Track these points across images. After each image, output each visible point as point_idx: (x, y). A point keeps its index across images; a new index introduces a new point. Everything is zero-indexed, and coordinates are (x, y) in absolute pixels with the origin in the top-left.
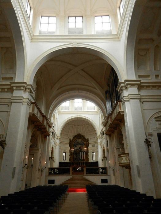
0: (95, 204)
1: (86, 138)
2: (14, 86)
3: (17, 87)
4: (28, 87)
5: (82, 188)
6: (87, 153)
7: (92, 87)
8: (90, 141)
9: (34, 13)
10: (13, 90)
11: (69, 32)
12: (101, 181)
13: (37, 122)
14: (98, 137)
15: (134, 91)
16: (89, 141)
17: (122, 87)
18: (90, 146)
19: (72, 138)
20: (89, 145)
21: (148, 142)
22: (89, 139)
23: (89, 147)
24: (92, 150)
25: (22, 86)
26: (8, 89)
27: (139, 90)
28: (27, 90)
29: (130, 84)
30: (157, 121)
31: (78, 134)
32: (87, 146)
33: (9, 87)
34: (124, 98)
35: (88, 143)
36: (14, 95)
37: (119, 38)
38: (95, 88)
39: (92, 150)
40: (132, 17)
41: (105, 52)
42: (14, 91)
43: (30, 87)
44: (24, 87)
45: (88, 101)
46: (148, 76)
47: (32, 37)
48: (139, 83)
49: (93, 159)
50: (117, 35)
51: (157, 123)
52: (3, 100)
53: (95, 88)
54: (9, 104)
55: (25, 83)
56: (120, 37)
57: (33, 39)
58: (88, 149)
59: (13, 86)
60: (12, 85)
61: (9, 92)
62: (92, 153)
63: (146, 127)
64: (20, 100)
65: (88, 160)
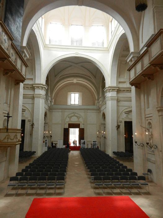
0: (88, 168)
2: (35, 87)
3: (37, 87)
4: (44, 87)
5: (141, 17)
7: (89, 76)
9: (45, 22)
10: (34, 98)
11: (72, 42)
12: (21, 121)
13: (12, 72)
15: (114, 94)
21: (118, 127)
25: (40, 87)
26: (31, 87)
27: (117, 93)
28: (43, 89)
29: (112, 89)
30: (125, 114)
33: (31, 86)
36: (35, 93)
37: (108, 50)
38: (90, 77)
40: (117, 43)
41: (98, 62)
42: (35, 90)
44: (41, 87)
46: (124, 82)
48: (118, 88)
50: (107, 48)
51: (125, 115)
52: (27, 95)
53: (90, 77)
54: (33, 98)
55: (41, 94)
56: (109, 50)
57: (45, 46)
59: (35, 87)
60: (34, 86)
61: (31, 89)
63: (118, 117)
64: (39, 96)
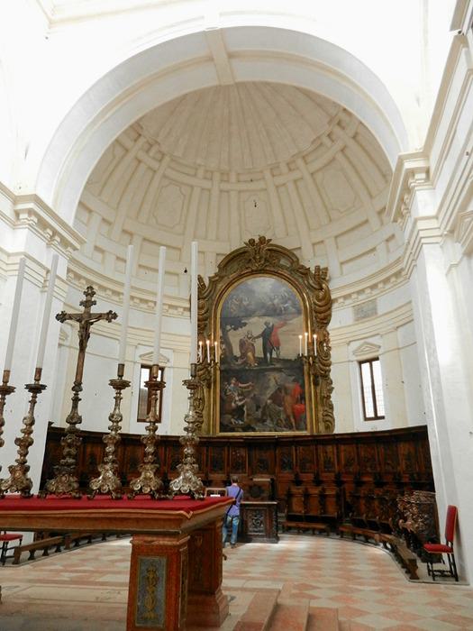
1: (310, 263)
6: (315, 369)
8: (336, 286)
14: (419, 164)
16: (332, 285)
17: (412, 172)
18: (340, 319)
19: (210, 271)
20: (334, 314)
22: (334, 271)
23: (330, 327)
24: (354, 345)
31: (252, 242)
32: (320, 316)
34: (421, 225)
35: (328, 293)
39: (354, 345)
43: (31, 205)
45: (257, 279)
47: (48, 18)
49: (370, 414)
58: (324, 340)
62: (361, 363)
65: (329, 423)
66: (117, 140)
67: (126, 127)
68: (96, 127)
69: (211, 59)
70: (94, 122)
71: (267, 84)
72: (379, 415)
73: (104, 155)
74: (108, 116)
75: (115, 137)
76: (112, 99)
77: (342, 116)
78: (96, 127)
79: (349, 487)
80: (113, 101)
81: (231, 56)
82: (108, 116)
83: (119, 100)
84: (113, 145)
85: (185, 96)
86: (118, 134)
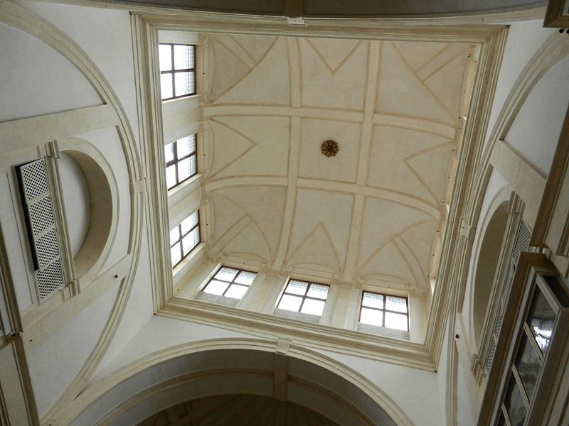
66: (165, 412)
67: (178, 403)
68: (153, 393)
69: (272, 375)
70: (153, 389)
71: (313, 412)
72: (363, 309)
73: (145, 421)
74: (167, 388)
75: (164, 408)
76: (170, 378)
77: (507, 263)
78: (153, 393)
79: (216, 248)
80: (170, 380)
81: (289, 378)
82: (167, 388)
83: (181, 379)
84: (159, 414)
85: (240, 395)
86: (168, 406)
